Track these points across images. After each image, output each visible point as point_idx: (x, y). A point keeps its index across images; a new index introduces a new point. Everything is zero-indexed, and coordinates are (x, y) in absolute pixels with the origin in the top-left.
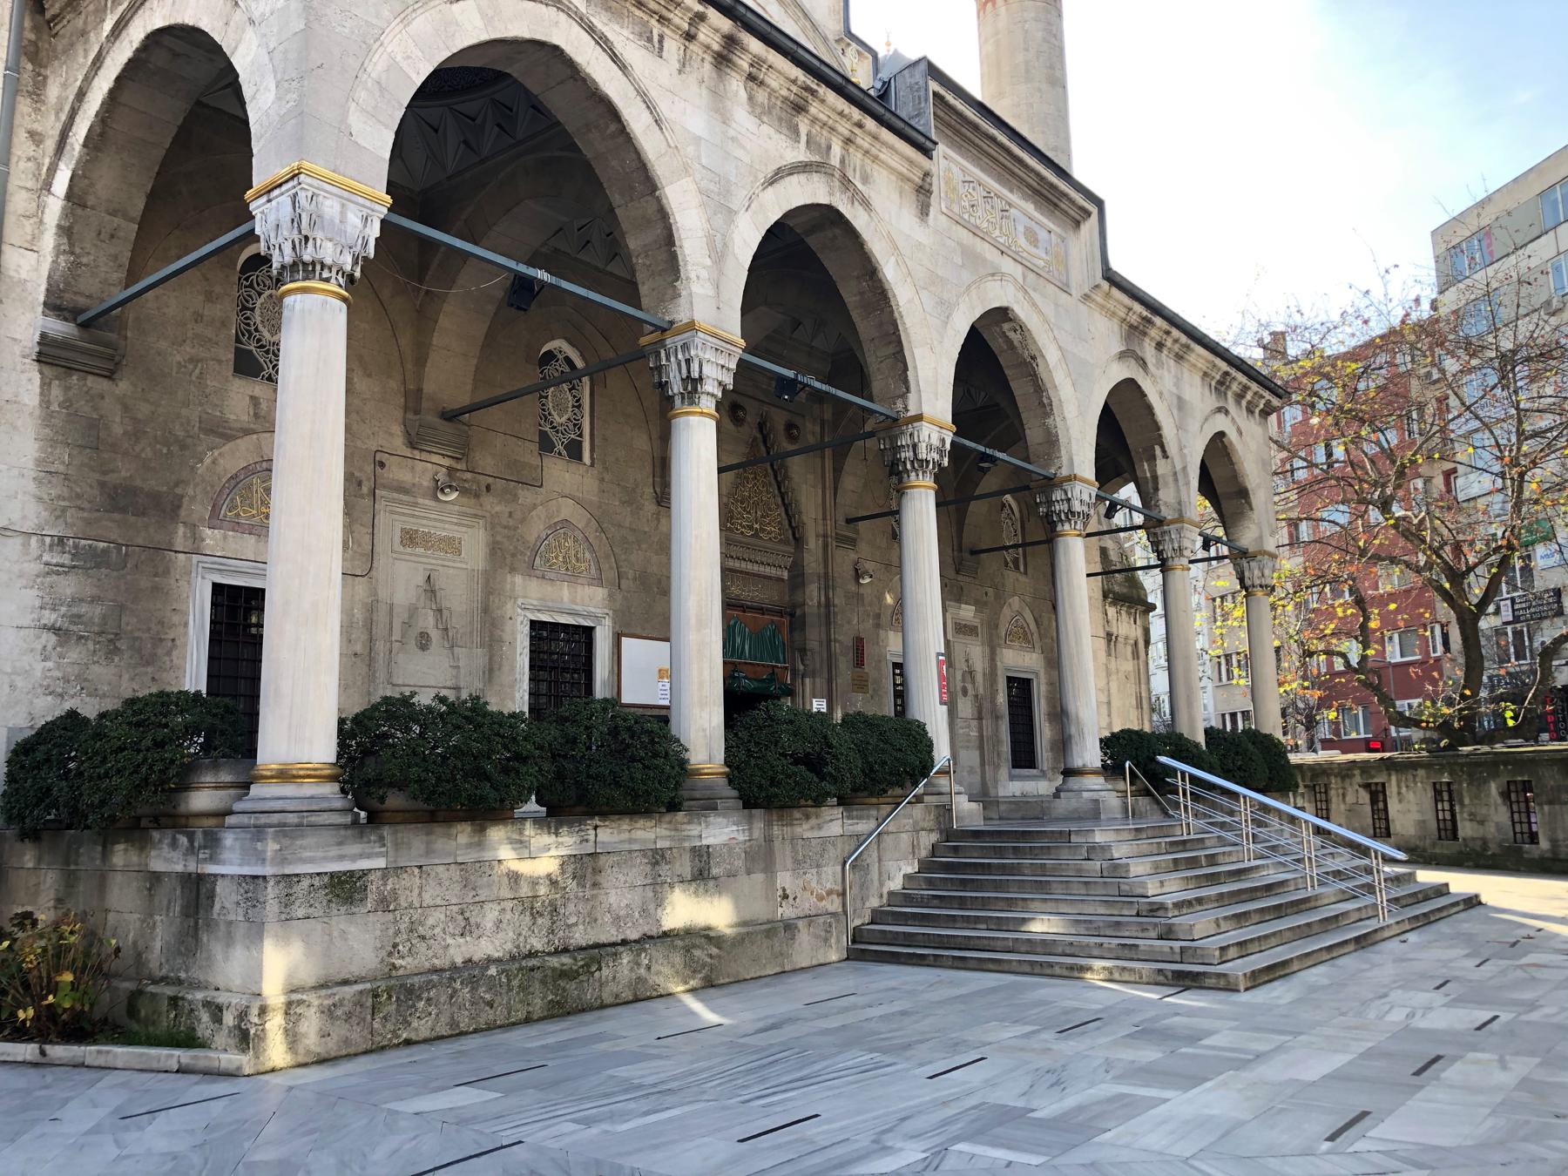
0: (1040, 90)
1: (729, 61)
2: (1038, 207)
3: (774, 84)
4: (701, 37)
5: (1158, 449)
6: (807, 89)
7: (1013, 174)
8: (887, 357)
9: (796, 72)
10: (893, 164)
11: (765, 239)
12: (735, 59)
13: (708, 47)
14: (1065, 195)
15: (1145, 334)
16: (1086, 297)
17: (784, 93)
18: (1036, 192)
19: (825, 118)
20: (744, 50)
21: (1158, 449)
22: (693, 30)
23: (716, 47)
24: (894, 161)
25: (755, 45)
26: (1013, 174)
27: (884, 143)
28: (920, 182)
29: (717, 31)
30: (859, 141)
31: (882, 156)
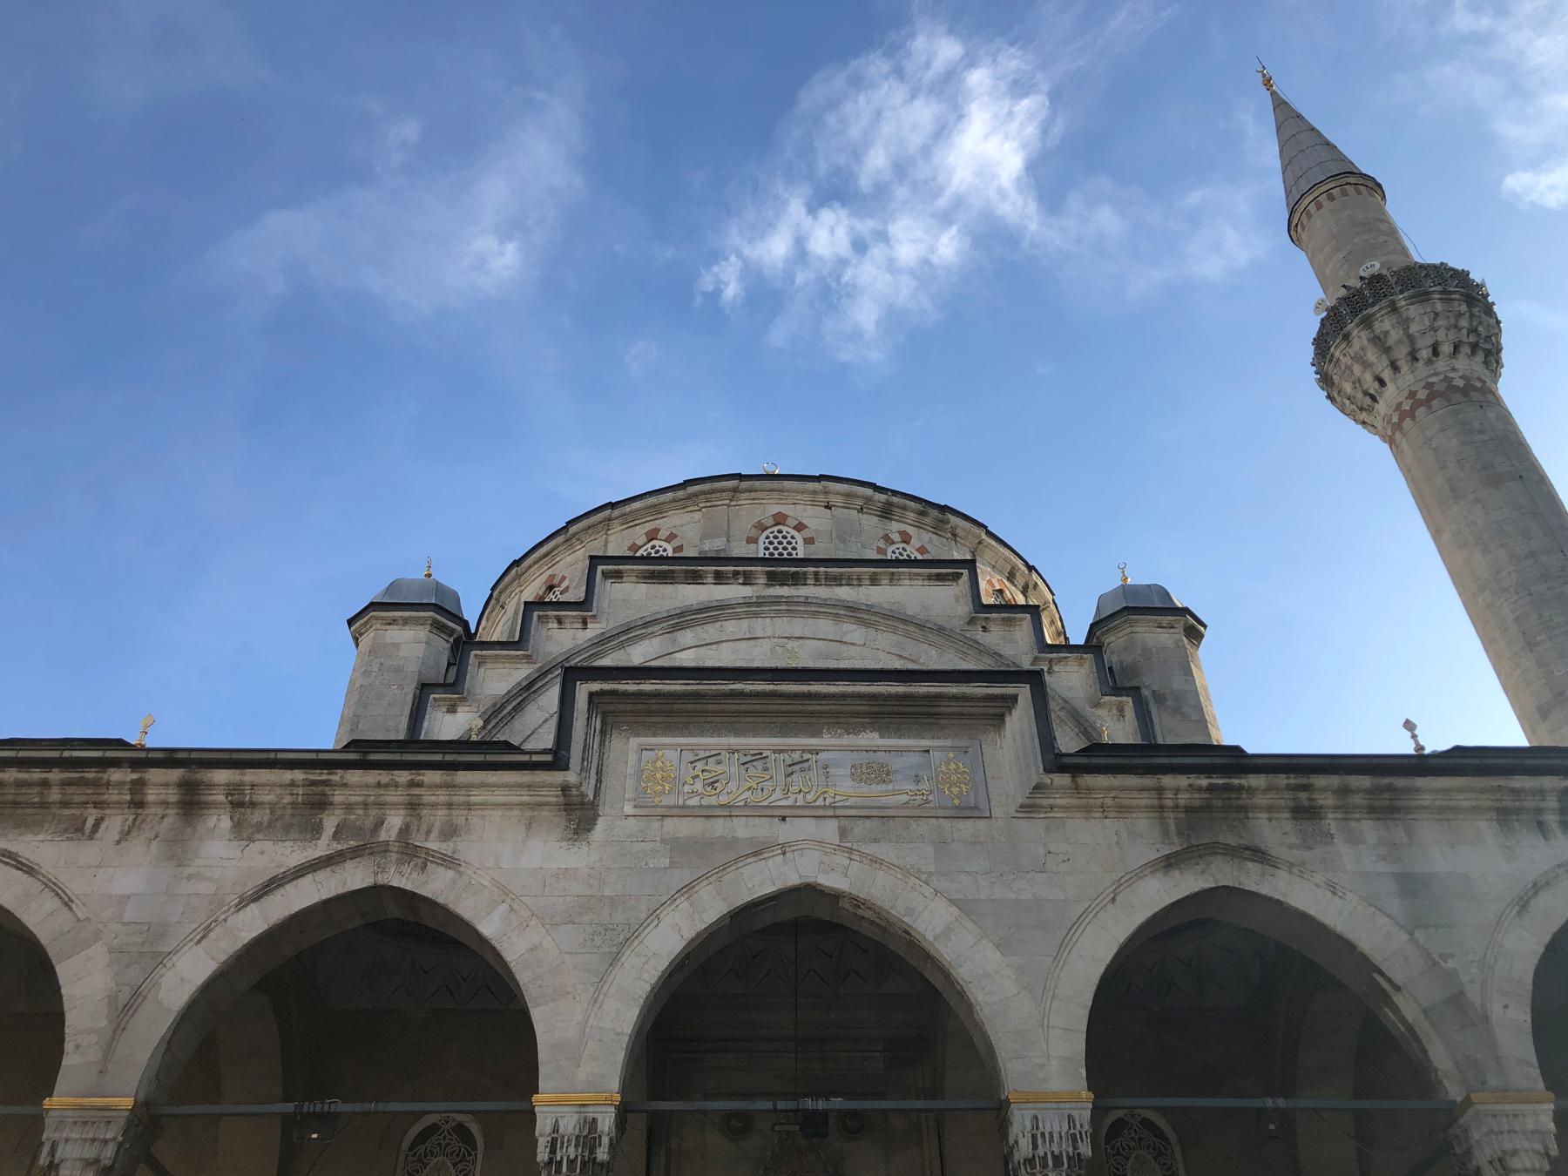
0: (1478, 500)
1: (199, 803)
2: (884, 732)
3: (267, 798)
4: (150, 798)
5: (1376, 975)
6: (313, 783)
7: (812, 714)
8: (1546, 1148)
9: (288, 775)
10: (501, 799)
11: (1535, 1036)
12: (203, 798)
13: (165, 804)
14: (939, 696)
15: (1244, 809)
16: (1028, 809)
17: (287, 799)
18: (874, 715)
19: (360, 799)
20: (212, 786)
21: (1376, 975)
22: (138, 797)
23: (173, 799)
24: (500, 797)
25: (222, 776)
26: (812, 714)
27: (469, 786)
28: (561, 799)
29: (167, 785)
30: (427, 799)
31: (474, 799)
